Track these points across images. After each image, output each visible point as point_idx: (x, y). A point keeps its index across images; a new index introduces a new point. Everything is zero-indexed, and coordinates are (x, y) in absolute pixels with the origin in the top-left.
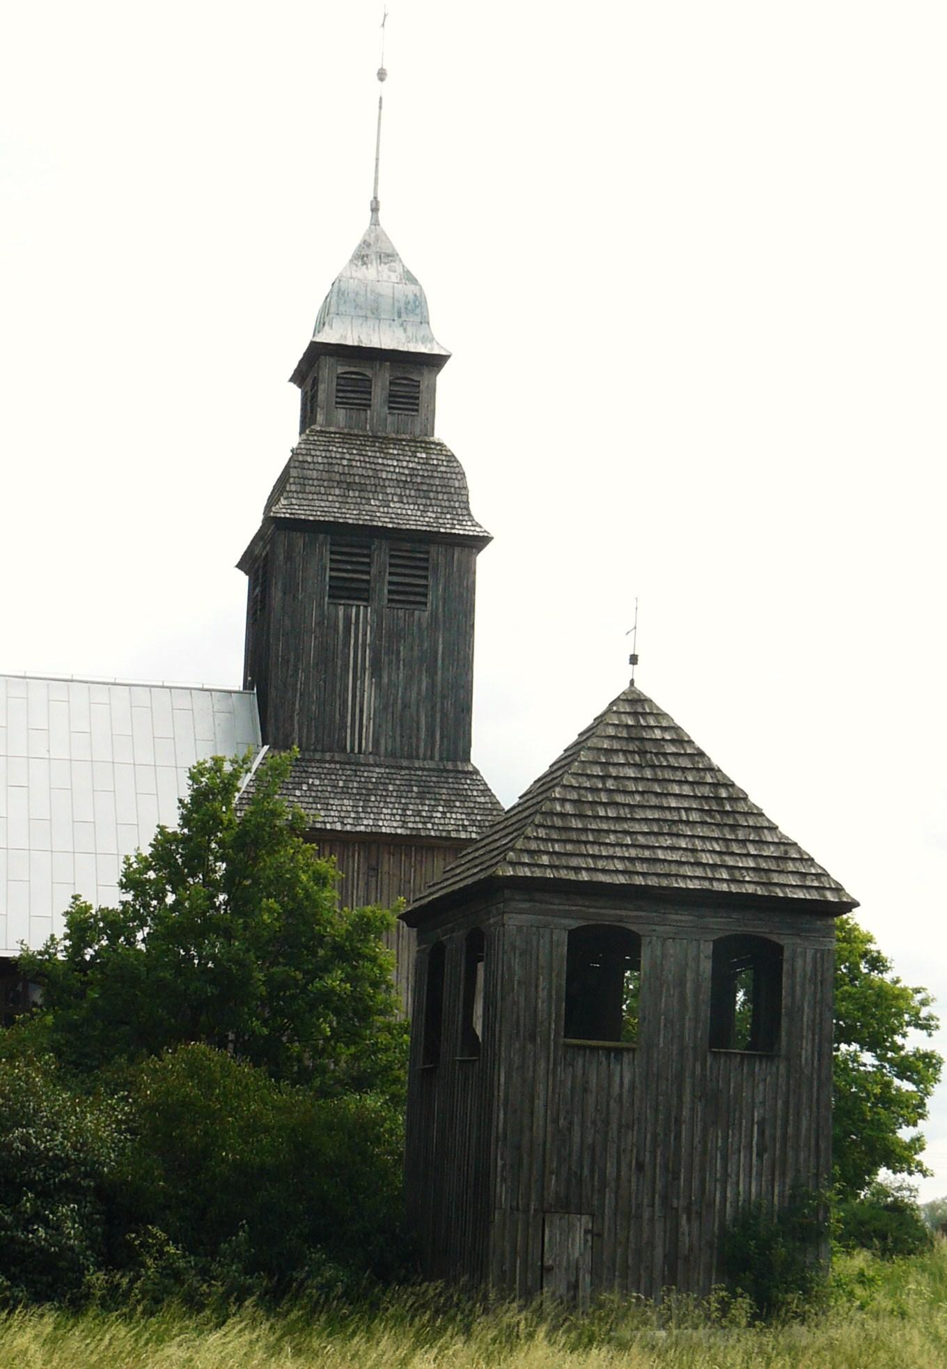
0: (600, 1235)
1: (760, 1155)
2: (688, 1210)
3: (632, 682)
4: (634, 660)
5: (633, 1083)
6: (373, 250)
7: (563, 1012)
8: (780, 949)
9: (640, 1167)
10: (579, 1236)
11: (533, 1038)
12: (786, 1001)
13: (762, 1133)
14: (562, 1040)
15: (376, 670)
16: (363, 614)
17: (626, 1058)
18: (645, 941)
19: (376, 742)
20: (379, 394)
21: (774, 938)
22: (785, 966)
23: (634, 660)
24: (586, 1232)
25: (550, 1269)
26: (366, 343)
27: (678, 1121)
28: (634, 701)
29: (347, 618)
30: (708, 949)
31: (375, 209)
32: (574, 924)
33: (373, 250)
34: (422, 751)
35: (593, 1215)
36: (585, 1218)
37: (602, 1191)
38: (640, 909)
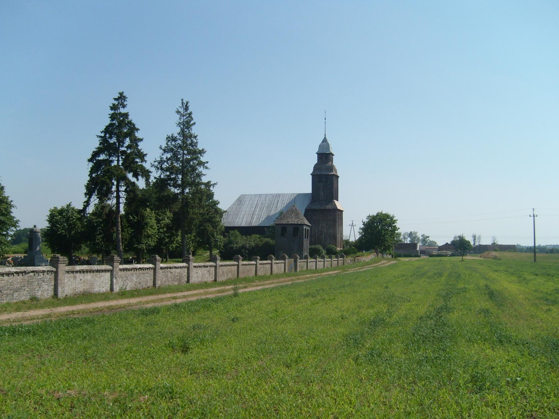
6: (325, 140)
33: (325, 140)
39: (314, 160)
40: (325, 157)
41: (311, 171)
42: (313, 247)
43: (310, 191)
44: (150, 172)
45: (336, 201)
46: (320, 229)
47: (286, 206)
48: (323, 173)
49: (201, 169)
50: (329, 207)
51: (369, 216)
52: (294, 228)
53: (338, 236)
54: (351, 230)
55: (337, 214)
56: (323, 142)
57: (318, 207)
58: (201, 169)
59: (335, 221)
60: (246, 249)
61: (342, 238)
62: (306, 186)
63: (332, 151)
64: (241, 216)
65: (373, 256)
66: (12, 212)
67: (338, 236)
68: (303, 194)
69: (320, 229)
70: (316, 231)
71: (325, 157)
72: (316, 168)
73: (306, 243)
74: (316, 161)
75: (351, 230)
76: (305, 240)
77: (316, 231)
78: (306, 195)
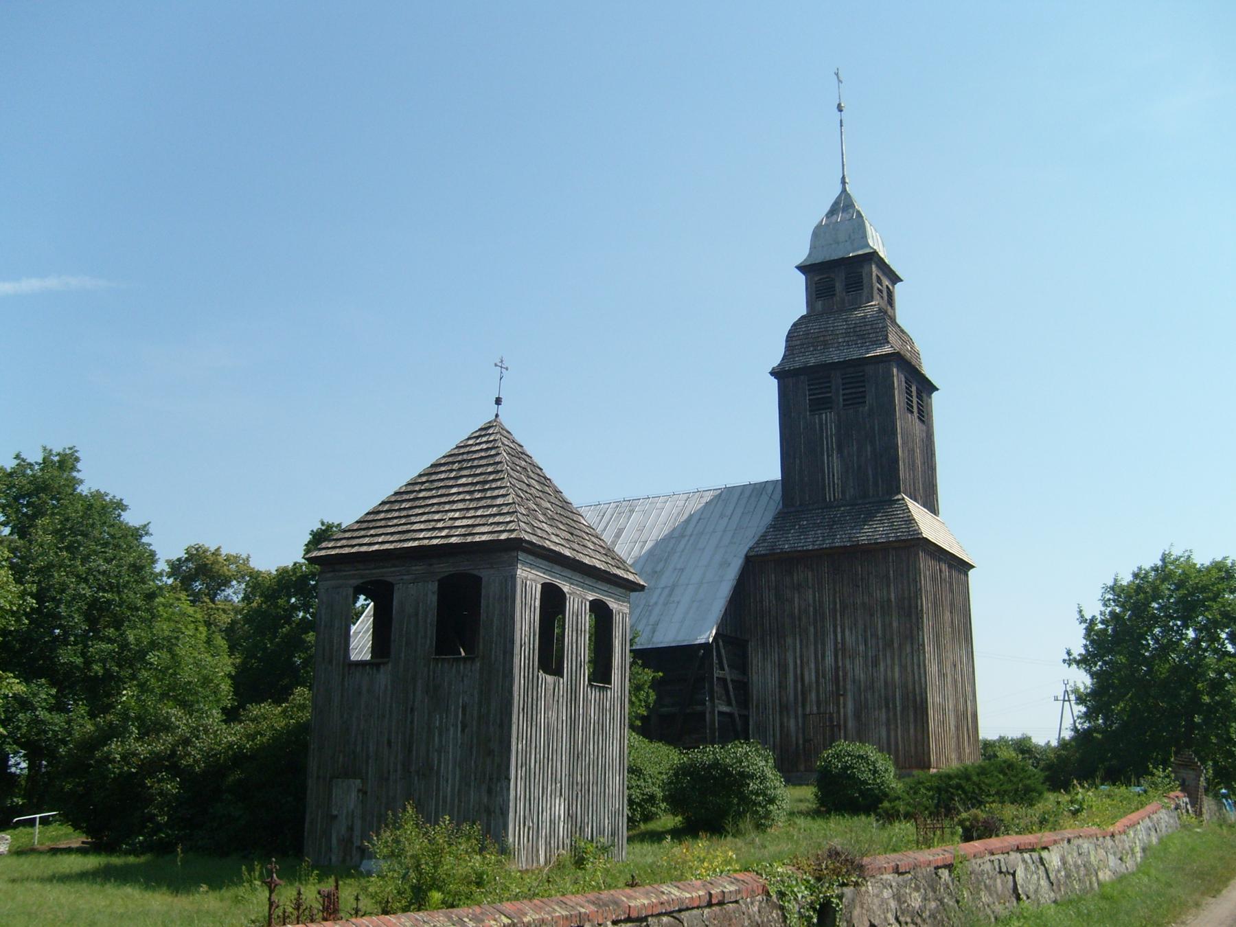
0: (365, 793)
1: (463, 731)
3: (497, 416)
4: (498, 401)
6: (843, 204)
8: (480, 579)
10: (354, 794)
11: (331, 662)
12: (483, 617)
13: (464, 714)
16: (829, 417)
17: (382, 669)
18: (396, 588)
19: (843, 493)
20: (839, 286)
21: (475, 572)
23: (498, 401)
24: (359, 791)
25: (336, 816)
29: (821, 420)
30: (434, 587)
31: (843, 182)
33: (843, 204)
34: (871, 493)
39: (792, 301)
40: (845, 278)
41: (775, 354)
45: (917, 511)
46: (829, 660)
47: (651, 552)
48: (835, 356)
49: (145, 540)
50: (875, 531)
56: (833, 212)
57: (811, 541)
58: (145, 540)
59: (910, 612)
61: (968, 718)
62: (748, 448)
63: (876, 241)
65: (1165, 818)
66: (81, 482)
67: (940, 722)
69: (829, 660)
70: (809, 676)
71: (845, 278)
72: (798, 337)
74: (799, 308)
77: (809, 676)
78: (758, 490)
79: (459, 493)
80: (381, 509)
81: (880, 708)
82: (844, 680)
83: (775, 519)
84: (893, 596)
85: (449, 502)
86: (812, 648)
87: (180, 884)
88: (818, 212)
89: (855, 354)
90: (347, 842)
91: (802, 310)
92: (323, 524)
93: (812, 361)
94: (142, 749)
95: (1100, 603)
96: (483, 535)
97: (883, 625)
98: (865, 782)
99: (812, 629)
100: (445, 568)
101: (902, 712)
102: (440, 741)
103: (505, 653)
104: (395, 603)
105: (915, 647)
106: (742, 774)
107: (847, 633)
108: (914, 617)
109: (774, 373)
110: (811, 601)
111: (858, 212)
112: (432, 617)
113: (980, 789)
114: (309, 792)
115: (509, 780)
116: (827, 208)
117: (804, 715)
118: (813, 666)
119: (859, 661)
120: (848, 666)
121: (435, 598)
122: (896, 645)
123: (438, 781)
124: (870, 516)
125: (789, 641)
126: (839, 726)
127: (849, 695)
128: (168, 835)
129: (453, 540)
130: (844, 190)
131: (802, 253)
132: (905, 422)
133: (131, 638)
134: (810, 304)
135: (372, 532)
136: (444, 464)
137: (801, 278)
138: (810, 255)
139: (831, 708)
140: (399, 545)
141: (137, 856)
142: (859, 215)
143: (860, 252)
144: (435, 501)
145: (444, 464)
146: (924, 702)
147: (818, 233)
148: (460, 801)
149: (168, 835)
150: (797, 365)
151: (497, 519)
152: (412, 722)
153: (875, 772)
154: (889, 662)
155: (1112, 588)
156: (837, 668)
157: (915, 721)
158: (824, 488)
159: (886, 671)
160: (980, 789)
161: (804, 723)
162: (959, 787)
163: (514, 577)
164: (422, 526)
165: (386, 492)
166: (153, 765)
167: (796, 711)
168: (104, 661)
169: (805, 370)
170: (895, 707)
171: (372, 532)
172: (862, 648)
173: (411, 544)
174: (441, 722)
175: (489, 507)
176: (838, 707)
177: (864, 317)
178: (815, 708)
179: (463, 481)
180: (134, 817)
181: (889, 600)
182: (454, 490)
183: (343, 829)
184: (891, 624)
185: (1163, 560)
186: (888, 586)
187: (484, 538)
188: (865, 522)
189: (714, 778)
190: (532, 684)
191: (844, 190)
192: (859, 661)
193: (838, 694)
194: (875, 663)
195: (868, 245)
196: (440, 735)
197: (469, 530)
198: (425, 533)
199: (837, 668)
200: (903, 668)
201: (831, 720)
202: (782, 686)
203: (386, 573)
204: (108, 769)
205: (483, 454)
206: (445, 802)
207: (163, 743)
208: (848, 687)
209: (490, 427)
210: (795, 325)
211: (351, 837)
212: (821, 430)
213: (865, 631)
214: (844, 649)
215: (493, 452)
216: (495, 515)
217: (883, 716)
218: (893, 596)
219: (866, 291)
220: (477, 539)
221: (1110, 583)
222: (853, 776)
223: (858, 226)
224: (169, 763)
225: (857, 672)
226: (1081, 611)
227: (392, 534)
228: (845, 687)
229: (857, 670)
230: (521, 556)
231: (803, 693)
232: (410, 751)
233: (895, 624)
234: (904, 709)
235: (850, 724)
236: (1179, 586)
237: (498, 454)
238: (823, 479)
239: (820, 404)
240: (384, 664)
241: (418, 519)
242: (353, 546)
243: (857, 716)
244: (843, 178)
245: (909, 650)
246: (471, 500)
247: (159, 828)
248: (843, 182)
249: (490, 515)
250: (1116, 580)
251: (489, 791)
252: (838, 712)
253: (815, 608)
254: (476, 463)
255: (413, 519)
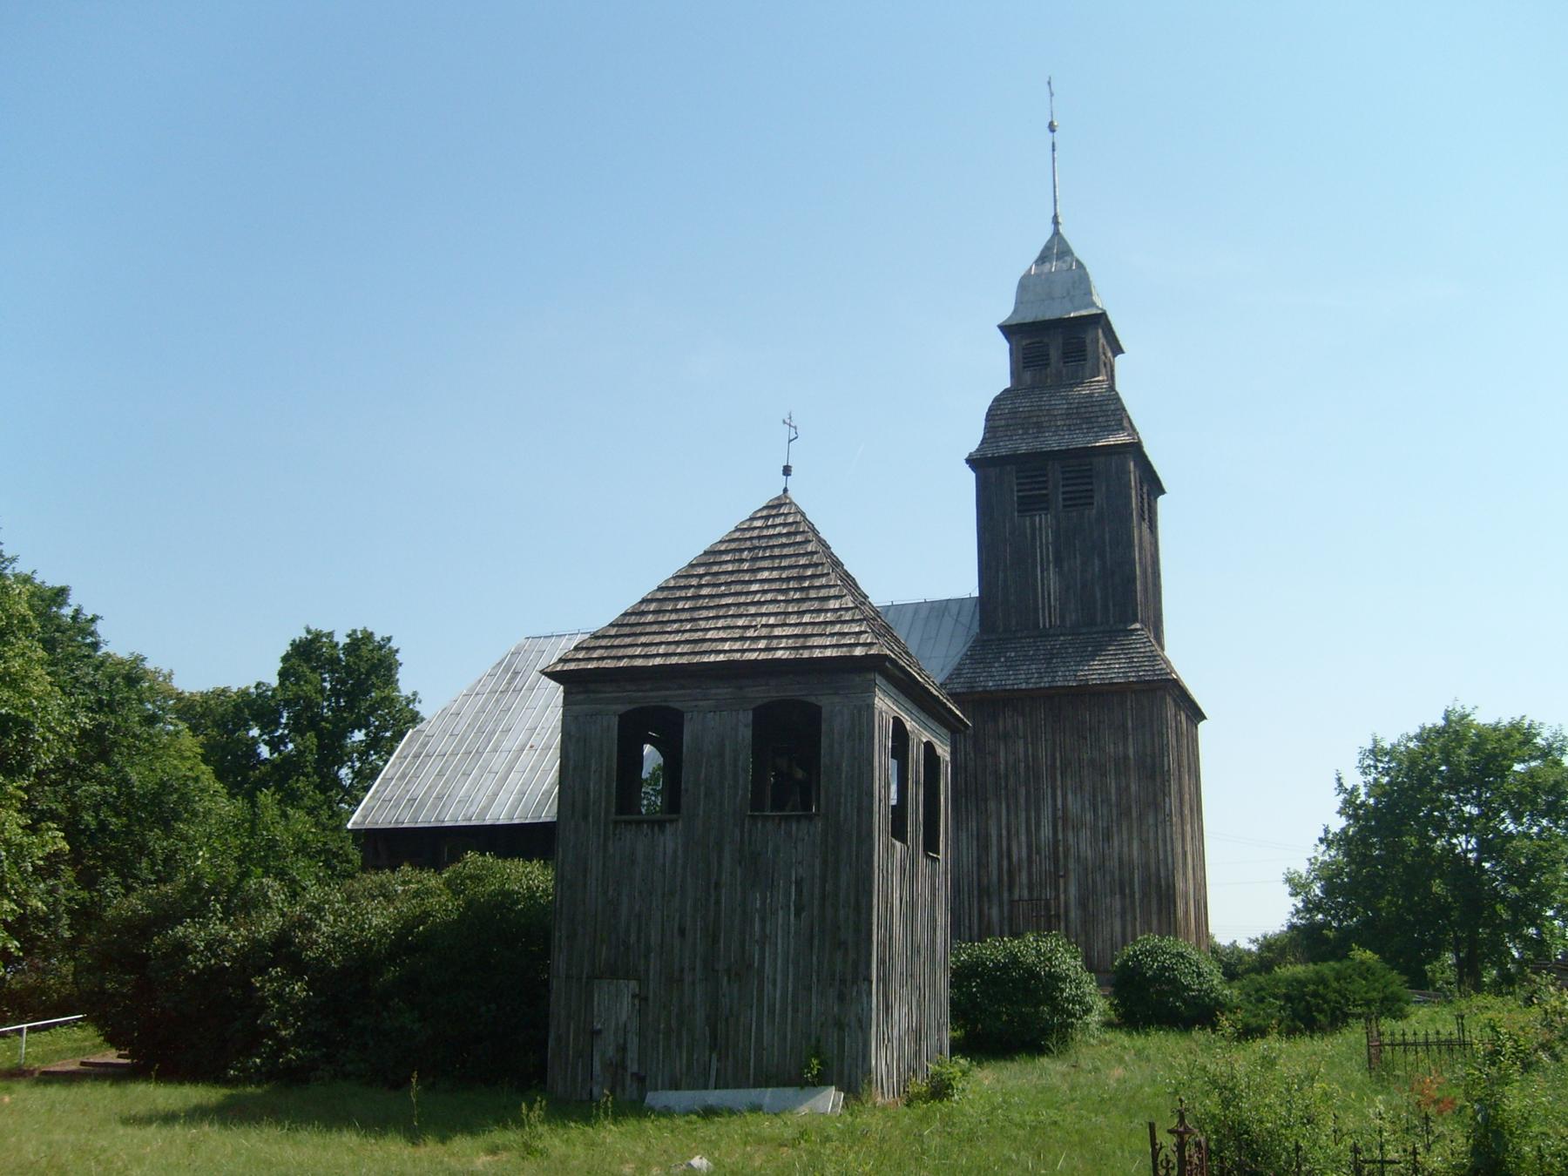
0: (646, 999)
1: (797, 915)
2: (728, 971)
3: (785, 490)
4: (787, 471)
5: (675, 852)
6: (1056, 249)
7: (614, 791)
8: (817, 710)
9: (682, 932)
10: (626, 1001)
11: (585, 817)
12: (824, 760)
13: (799, 892)
14: (613, 817)
15: (1058, 561)
17: (669, 828)
18: (687, 717)
19: (1063, 618)
20: (1054, 354)
21: (812, 699)
22: (824, 727)
23: (787, 471)
24: (634, 996)
25: (599, 1032)
26: (1040, 318)
27: (717, 885)
28: (778, 506)
31: (1056, 222)
32: (622, 708)
33: (1056, 249)
35: (639, 980)
36: (633, 984)
37: (647, 957)
38: (683, 688)
39: (995, 369)
40: (1059, 345)
41: (972, 436)
42: (994, 950)
43: (976, 594)
44: (957, 1048)
46: (1046, 832)
48: (1053, 443)
50: (1106, 668)
51: (1376, 752)
52: (765, 719)
53: (1180, 885)
54: (1254, 867)
55: (1158, 714)
56: (1043, 259)
57: (1024, 677)
60: (297, 967)
63: (1105, 298)
64: (499, 762)
68: (917, 607)
69: (1046, 832)
70: (1020, 852)
71: (1059, 345)
72: (1000, 416)
73: (909, 899)
75: (1254, 867)
76: (889, 858)
77: (1020, 852)
79: (764, 592)
80: (644, 608)
81: (1113, 893)
82: (1066, 857)
83: (972, 648)
84: (1131, 751)
85: (753, 603)
86: (1023, 815)
87: (446, 1126)
88: (1024, 258)
89: (1080, 441)
90: (617, 1068)
91: (1005, 382)
92: (308, 632)
93: (1023, 448)
94: (238, 937)
95: (1358, 772)
96: (824, 648)
97: (1118, 788)
98: (1188, 988)
99: (1023, 791)
100: (761, 693)
101: (1142, 901)
102: (763, 929)
103: (859, 810)
104: (686, 738)
105: (1160, 817)
106: (1049, 975)
107: (1070, 797)
108: (1159, 780)
109: (973, 462)
110: (1021, 756)
111: (1078, 261)
112: (746, 759)
113: (1344, 996)
114: (553, 998)
115: (871, 982)
116: (1036, 255)
117: (1012, 902)
118: (1023, 838)
119: (1085, 834)
120: (1071, 841)
121: (748, 733)
122: (1134, 815)
123: (761, 982)
124: (1099, 649)
125: (992, 805)
126: (1058, 916)
127: (1072, 877)
128: (298, 1056)
129: (779, 654)
130: (1056, 233)
131: (1005, 309)
132: (1139, 531)
133: (134, 777)
134: (1015, 374)
135: (643, 639)
136: (726, 552)
137: (1003, 346)
138: (1015, 311)
139: (1049, 893)
140: (696, 659)
141: (258, 1085)
142: (1080, 265)
143: (1084, 313)
144: (730, 600)
145: (726, 552)
146: (1171, 887)
147: (1025, 285)
148: (795, 1010)
149: (298, 1056)
150: (1003, 452)
151: (837, 628)
152: (718, 902)
153: (1199, 975)
154: (1125, 836)
155: (1372, 751)
156: (1056, 841)
157: (1160, 911)
158: (1036, 610)
159: (1121, 847)
160: (1344, 996)
161: (1011, 911)
162: (1315, 994)
163: (871, 707)
164: (722, 634)
165: (647, 587)
166: (256, 958)
167: (1000, 895)
168: (96, 808)
169: (1013, 459)
170: (1132, 895)
171: (643, 639)
172: (1089, 817)
173: (712, 658)
174: (763, 903)
175: (819, 611)
176: (1057, 889)
177: (1091, 395)
178: (1025, 893)
179: (765, 575)
180: (179, 1022)
181: (1126, 757)
182: (755, 587)
183: (611, 1052)
184: (1128, 787)
185: (1446, 718)
186: (1125, 739)
187: (828, 653)
188: (1093, 657)
189: (1013, 980)
190: (890, 849)
191: (1056, 233)
192: (1085, 834)
193: (1057, 875)
194: (1108, 838)
195: (1093, 304)
196: (763, 920)
197: (800, 642)
198: (724, 642)
199: (1056, 841)
200: (1144, 844)
201: (1048, 908)
202: (982, 864)
203: (674, 697)
204: (187, 963)
205: (784, 540)
206: (772, 1011)
207: (268, 925)
208: (1071, 866)
209: (780, 506)
210: (996, 400)
211: (623, 1060)
212: (1034, 538)
213: (1094, 796)
214: (1065, 819)
215: (799, 538)
216: (832, 623)
217: (1117, 905)
218: (1131, 751)
219: (1089, 364)
220: (817, 653)
221: (1369, 746)
222: (1174, 981)
223: (1080, 281)
224: (283, 950)
225: (1083, 846)
226: (1339, 779)
227: (678, 643)
228: (1066, 866)
229: (1083, 845)
230: (879, 680)
231: (1010, 871)
232: (715, 940)
233: (1133, 788)
234: (1145, 895)
235: (1074, 914)
236: (1475, 749)
237: (807, 541)
238: (1036, 601)
239: (1029, 505)
240: (671, 821)
241: (711, 624)
242: (620, 658)
243: (1083, 904)
244: (1055, 217)
245: (1151, 821)
246: (787, 602)
247: (283, 1045)
248: (1056, 222)
249: (826, 623)
250: (1375, 741)
251: (841, 998)
252: (1057, 897)
253: (1027, 767)
254: (777, 552)
255: (703, 624)
